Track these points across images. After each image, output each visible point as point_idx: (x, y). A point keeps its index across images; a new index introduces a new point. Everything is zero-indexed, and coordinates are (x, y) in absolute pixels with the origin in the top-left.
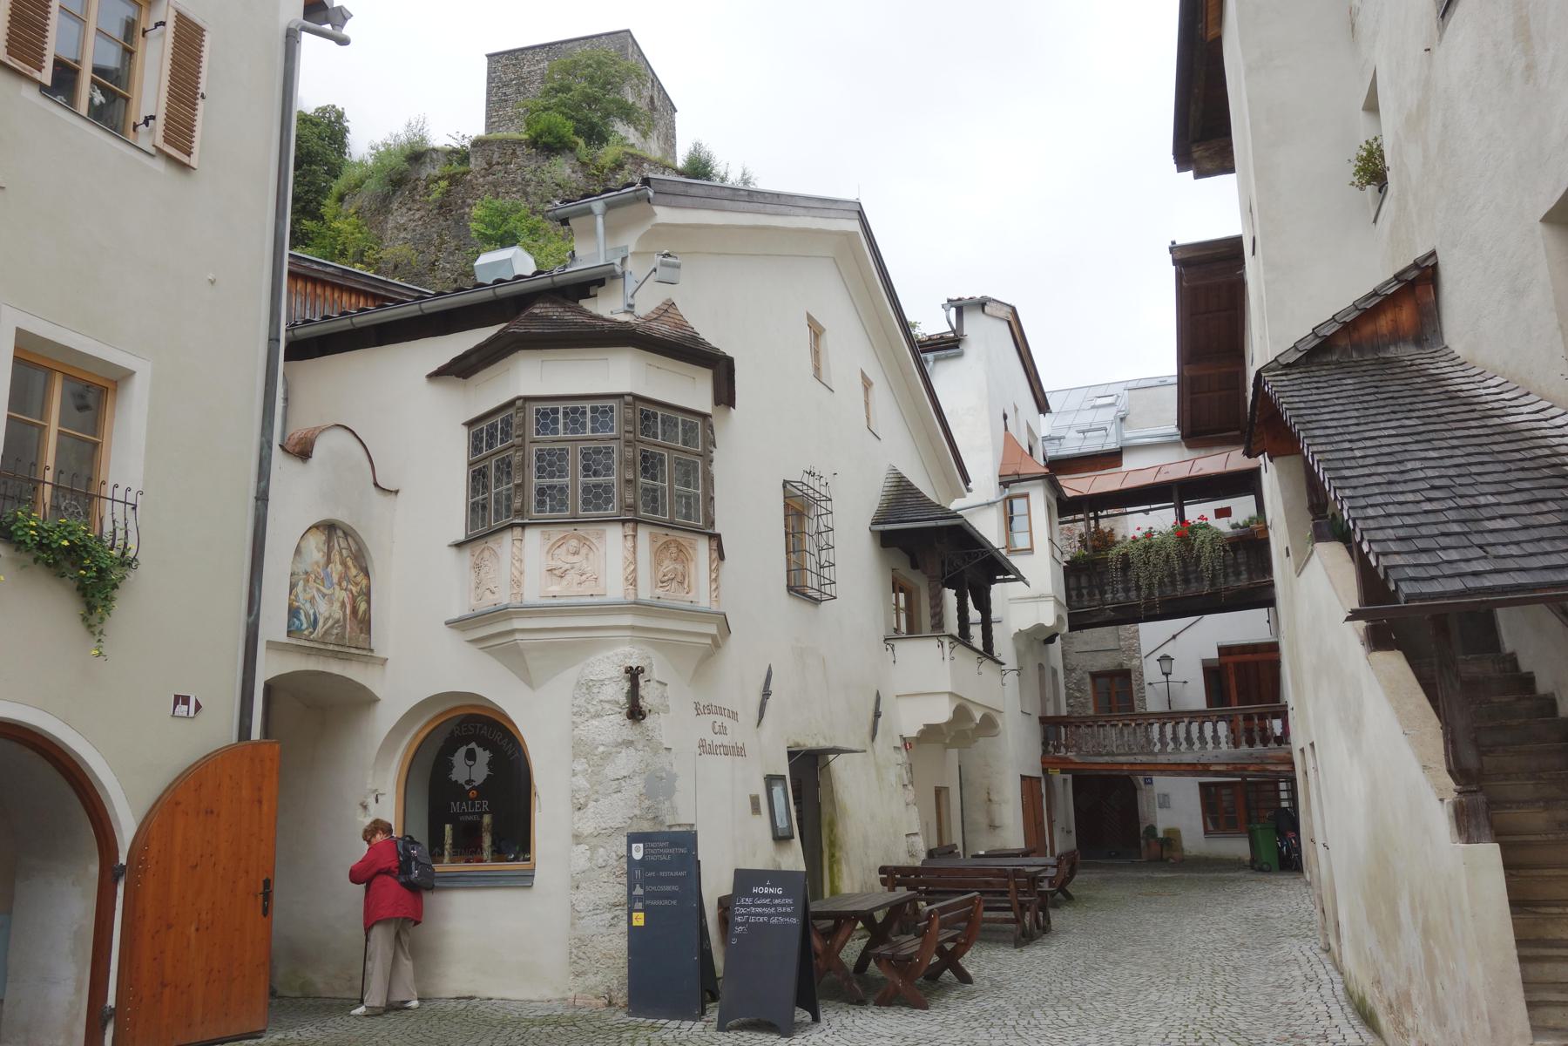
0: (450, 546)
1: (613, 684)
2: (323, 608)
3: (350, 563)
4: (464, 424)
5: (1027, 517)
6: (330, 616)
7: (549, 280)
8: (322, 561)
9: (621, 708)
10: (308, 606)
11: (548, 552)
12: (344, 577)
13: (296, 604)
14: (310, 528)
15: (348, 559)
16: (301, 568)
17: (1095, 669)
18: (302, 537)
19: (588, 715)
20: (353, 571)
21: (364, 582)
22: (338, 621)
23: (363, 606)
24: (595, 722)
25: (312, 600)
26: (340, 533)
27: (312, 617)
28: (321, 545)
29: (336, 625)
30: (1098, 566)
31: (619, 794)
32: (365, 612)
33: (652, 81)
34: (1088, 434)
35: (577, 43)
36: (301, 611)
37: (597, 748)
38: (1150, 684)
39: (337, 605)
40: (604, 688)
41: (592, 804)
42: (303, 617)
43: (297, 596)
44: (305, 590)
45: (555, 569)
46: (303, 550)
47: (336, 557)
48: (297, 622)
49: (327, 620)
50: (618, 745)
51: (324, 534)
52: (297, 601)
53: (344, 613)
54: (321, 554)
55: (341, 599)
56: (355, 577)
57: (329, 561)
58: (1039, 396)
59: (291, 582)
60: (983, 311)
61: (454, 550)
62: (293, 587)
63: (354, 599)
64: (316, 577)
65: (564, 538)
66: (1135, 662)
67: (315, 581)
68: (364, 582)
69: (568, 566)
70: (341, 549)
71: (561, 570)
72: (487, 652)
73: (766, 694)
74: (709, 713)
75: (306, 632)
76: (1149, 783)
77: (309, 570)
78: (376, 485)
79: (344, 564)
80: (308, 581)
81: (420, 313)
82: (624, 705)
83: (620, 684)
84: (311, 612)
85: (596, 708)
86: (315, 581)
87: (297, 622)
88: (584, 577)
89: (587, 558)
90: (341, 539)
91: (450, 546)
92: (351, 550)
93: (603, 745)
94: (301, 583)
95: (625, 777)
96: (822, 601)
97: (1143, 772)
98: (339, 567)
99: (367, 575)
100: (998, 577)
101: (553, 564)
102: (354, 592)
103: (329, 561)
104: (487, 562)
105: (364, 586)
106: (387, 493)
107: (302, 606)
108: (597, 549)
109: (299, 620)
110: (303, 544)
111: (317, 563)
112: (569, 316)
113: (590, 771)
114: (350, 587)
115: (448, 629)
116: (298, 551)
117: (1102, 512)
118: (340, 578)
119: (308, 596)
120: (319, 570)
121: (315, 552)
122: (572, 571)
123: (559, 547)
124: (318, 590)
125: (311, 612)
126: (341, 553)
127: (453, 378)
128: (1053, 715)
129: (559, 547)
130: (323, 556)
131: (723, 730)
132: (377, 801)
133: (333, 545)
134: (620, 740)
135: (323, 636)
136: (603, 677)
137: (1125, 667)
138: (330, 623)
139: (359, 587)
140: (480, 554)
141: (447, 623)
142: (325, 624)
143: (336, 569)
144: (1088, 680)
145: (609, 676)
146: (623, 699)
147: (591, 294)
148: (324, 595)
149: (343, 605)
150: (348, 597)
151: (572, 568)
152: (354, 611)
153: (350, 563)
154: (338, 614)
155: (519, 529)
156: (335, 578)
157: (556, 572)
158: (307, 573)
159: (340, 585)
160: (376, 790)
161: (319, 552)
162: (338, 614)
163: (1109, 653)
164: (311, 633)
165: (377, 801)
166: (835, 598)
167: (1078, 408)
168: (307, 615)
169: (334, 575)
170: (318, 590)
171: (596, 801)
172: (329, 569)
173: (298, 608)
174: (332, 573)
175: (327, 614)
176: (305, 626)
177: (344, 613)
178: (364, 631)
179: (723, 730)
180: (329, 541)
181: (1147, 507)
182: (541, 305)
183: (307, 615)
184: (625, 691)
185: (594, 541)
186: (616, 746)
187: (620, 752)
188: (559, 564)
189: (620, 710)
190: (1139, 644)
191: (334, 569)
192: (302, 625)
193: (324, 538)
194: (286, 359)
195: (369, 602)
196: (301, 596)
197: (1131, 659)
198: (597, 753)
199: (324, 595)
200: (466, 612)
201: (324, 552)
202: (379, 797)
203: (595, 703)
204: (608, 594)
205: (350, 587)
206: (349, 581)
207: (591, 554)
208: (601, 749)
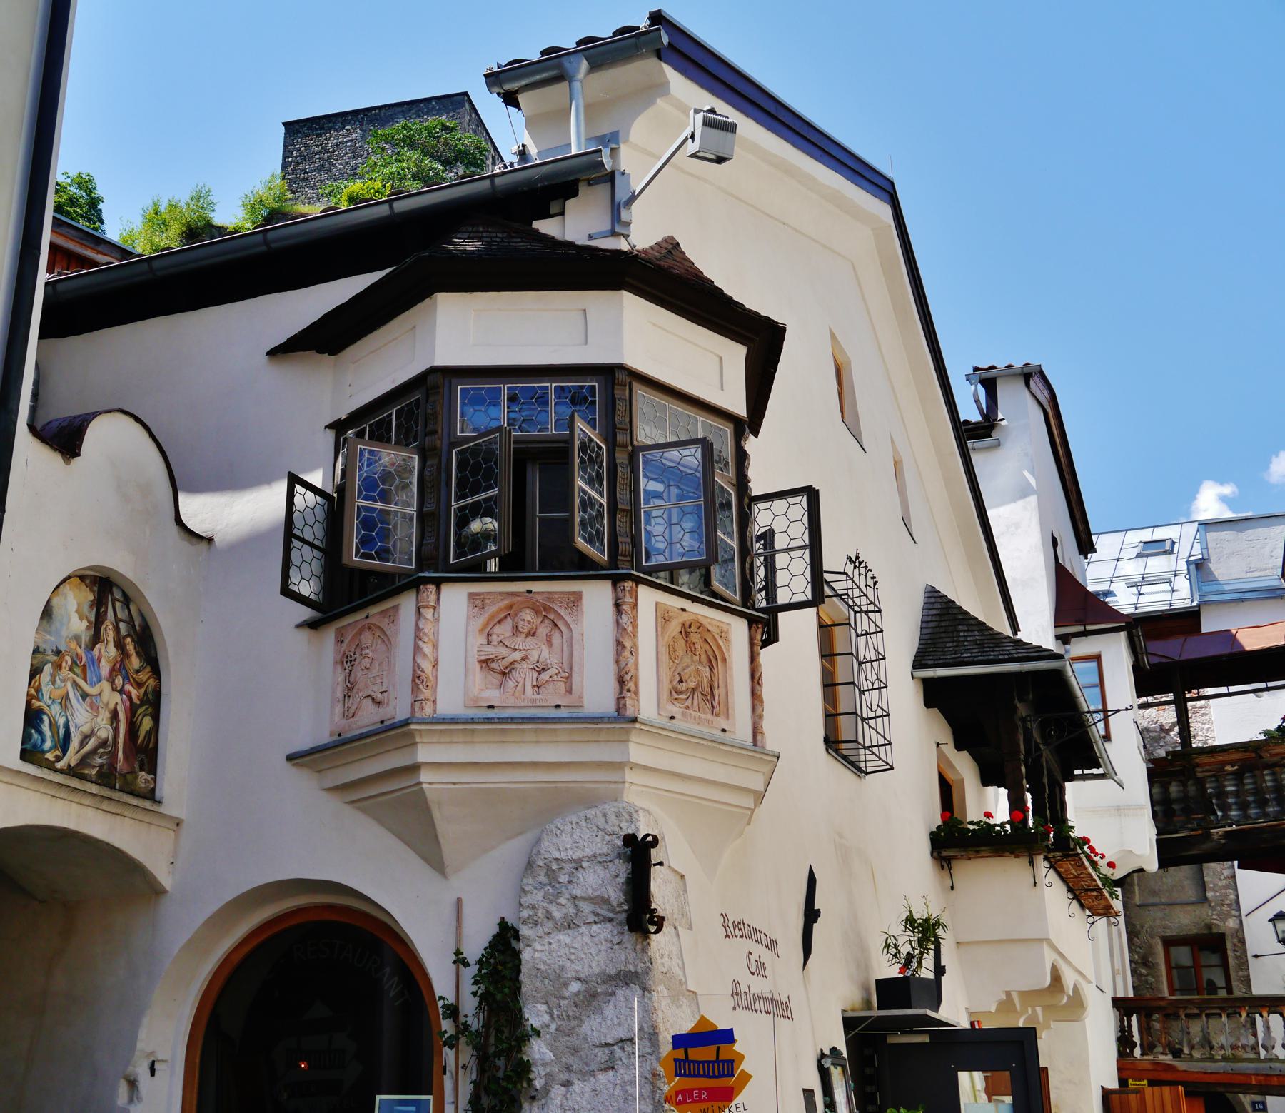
0: (298, 626)
1: (599, 869)
2: (81, 718)
3: (130, 647)
4: (329, 427)
5: (1098, 690)
6: (92, 734)
7: (487, 183)
8: (86, 637)
9: (613, 911)
10: (56, 710)
11: (481, 631)
12: (119, 668)
13: (36, 704)
14: (69, 577)
15: (129, 640)
16: (49, 642)
17: (1169, 933)
18: (55, 590)
19: (550, 924)
20: (135, 662)
21: (152, 683)
22: (104, 743)
23: (147, 724)
24: (564, 937)
25: (65, 701)
26: (118, 595)
27: (62, 731)
28: (86, 609)
29: (101, 750)
30: (1199, 770)
31: (611, 1073)
32: (148, 734)
33: (493, 158)
34: (1144, 589)
35: (399, 109)
36: (45, 718)
37: (566, 985)
38: (1256, 956)
39: (104, 716)
40: (580, 874)
41: (558, 1091)
42: (46, 728)
43: (38, 690)
44: (53, 682)
45: (493, 660)
46: (56, 611)
47: (109, 633)
48: (36, 736)
49: (85, 738)
50: (608, 979)
51: (91, 590)
52: (38, 700)
53: (116, 731)
54: (85, 623)
55: (112, 706)
56: (138, 671)
57: (96, 638)
58: (1081, 527)
59: (32, 665)
60: (1028, 385)
61: (306, 633)
62: (35, 672)
63: (132, 710)
64: (74, 662)
65: (510, 607)
66: (1232, 923)
67: (71, 669)
68: (152, 683)
69: (517, 656)
70: (117, 621)
71: (506, 662)
72: (359, 809)
73: (811, 915)
74: (741, 937)
75: (50, 756)
76: (1259, 1110)
77: (62, 648)
78: (179, 521)
79: (120, 645)
80: (60, 666)
81: (264, 248)
82: (619, 905)
83: (612, 868)
84: (61, 722)
85: (564, 911)
86: (71, 669)
87: (36, 736)
88: (545, 676)
89: (549, 643)
90: (118, 605)
91: (298, 626)
92: (134, 626)
93: (579, 979)
94: (48, 669)
95: (621, 1041)
96: (867, 773)
97: (1248, 1088)
98: (113, 651)
99: (156, 672)
100: (1078, 772)
101: (491, 651)
102: (134, 697)
103: (96, 638)
104: (367, 651)
105: (150, 689)
106: (194, 540)
107: (46, 709)
108: (569, 627)
109: (40, 732)
110: (55, 602)
111: (77, 638)
112: (517, 242)
113: (553, 1027)
114: (128, 687)
115: (294, 769)
116: (47, 613)
117: (1190, 692)
118: (113, 670)
119: (58, 693)
120: (79, 650)
121: (75, 618)
122: (524, 665)
123: (499, 622)
124: (75, 684)
125: (61, 722)
126: (117, 629)
127: (313, 353)
128: (1122, 996)
129: (499, 622)
130: (88, 628)
131: (759, 971)
132: (153, 1072)
133: (106, 612)
134: (613, 972)
135: (77, 765)
136: (578, 854)
137: (1215, 930)
138: (92, 743)
139: (142, 690)
140: (353, 639)
141: (290, 758)
142: (82, 745)
143: (107, 652)
144: (1160, 949)
145: (588, 852)
146: (615, 894)
147: (552, 211)
148: (85, 696)
149: (114, 716)
150: (125, 706)
151: (524, 659)
152: (133, 730)
153: (130, 647)
154: (105, 732)
155: (431, 588)
156: (105, 668)
157: (494, 665)
158: (58, 652)
159: (113, 683)
160: (152, 1053)
161: (81, 619)
162: (105, 732)
163: (1189, 908)
164: (58, 759)
165: (153, 1072)
166: (892, 768)
167: (1117, 557)
168: (53, 725)
169: (103, 662)
170: (75, 684)
171: (567, 1084)
172: (96, 651)
173: (40, 712)
174: (99, 659)
175: (86, 729)
176: (48, 745)
177: (116, 731)
178: (146, 767)
179: (759, 971)
180: (99, 604)
181: (1263, 685)
182: (470, 229)
183: (53, 725)
184: (622, 879)
185: (562, 612)
186: (604, 983)
187: (613, 994)
188: (502, 651)
189: (611, 915)
190: (1237, 896)
191: (103, 651)
192: (43, 741)
193: (91, 597)
194: (42, 335)
195: (156, 718)
196: (46, 691)
197: (1226, 916)
198: (567, 994)
199: (85, 696)
200: (324, 738)
201: (89, 622)
202: (157, 1066)
203: (562, 901)
204: (585, 703)
205: (128, 687)
206: (126, 678)
207: (556, 638)
208: (575, 987)
